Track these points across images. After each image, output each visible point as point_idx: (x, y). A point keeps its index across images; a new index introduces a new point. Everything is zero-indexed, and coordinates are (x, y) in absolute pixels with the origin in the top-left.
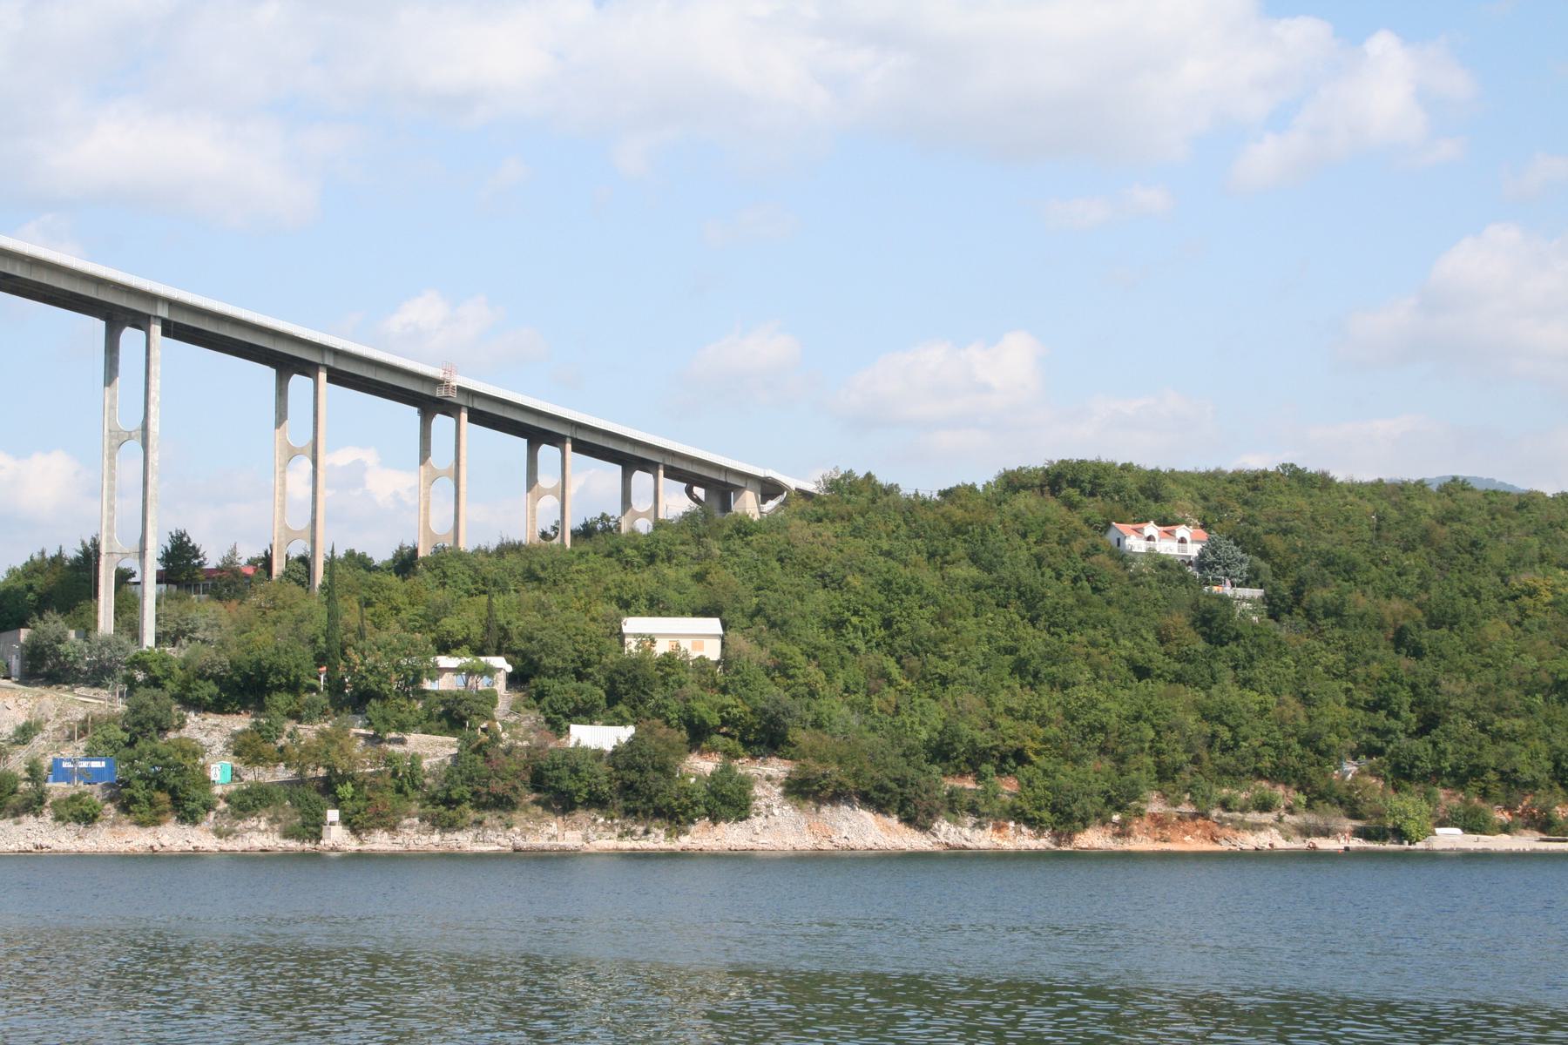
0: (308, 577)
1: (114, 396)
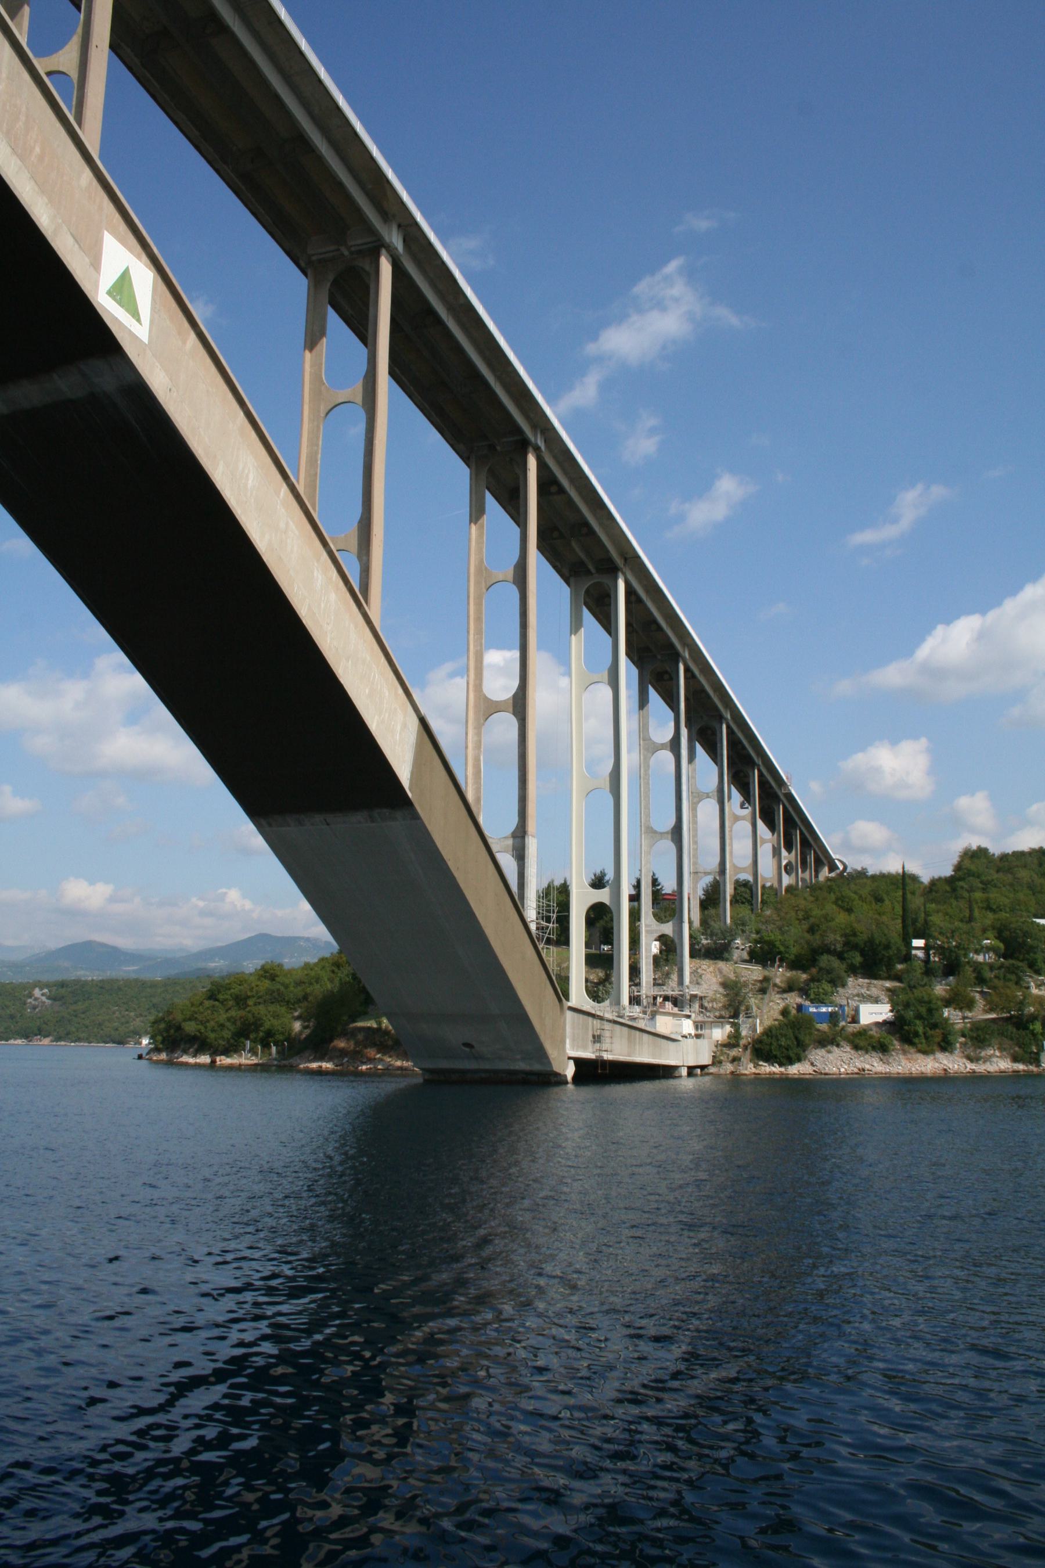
0: (752, 897)
1: (694, 770)
